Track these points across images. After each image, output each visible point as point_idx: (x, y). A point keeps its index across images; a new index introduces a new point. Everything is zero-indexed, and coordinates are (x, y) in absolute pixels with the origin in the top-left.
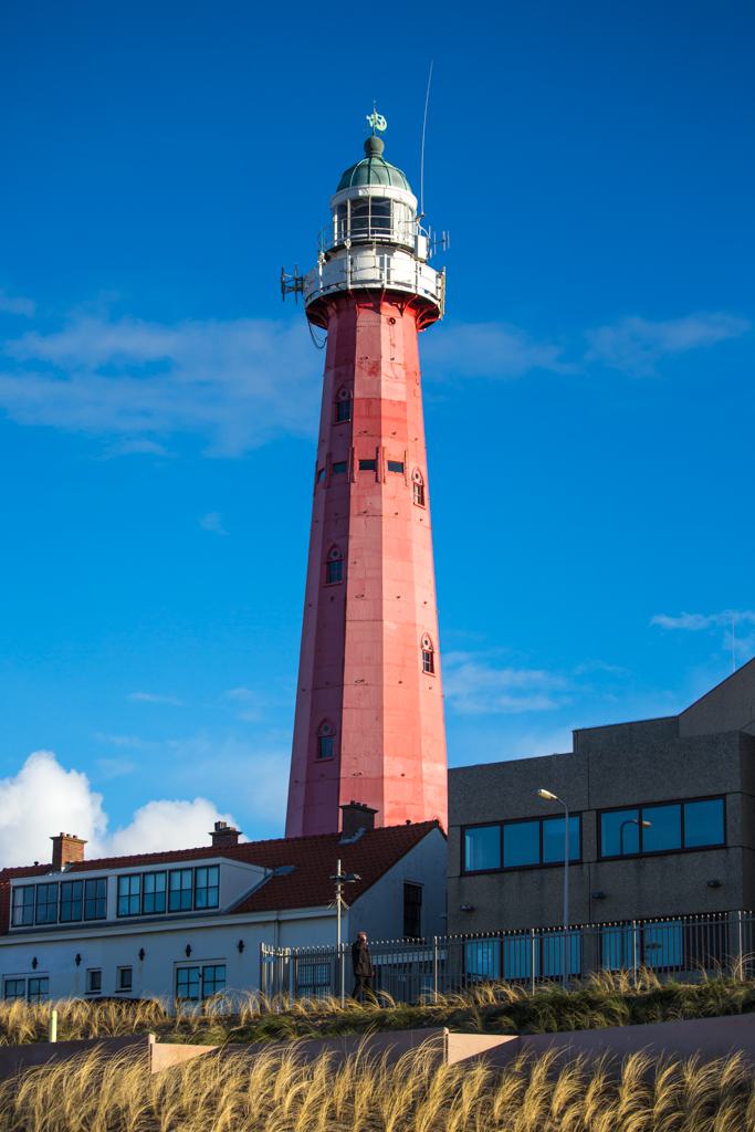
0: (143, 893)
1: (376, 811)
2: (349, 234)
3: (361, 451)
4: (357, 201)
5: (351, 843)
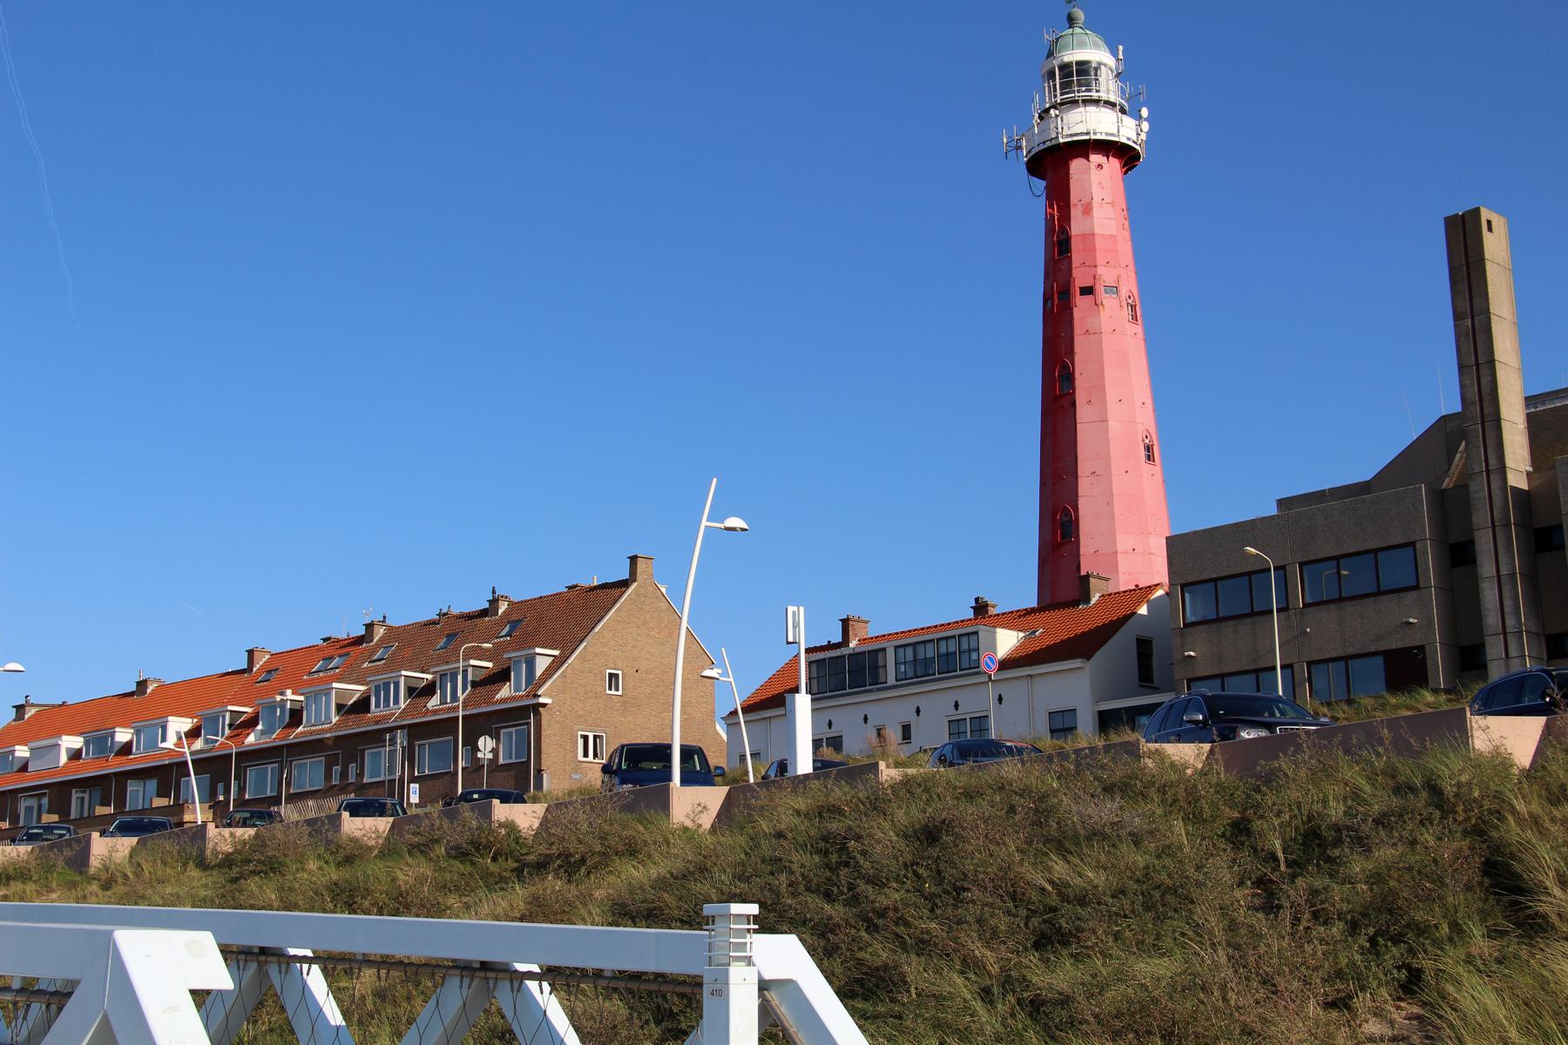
0: (915, 660)
2: (1058, 94)
3: (1080, 278)
4: (1065, 67)
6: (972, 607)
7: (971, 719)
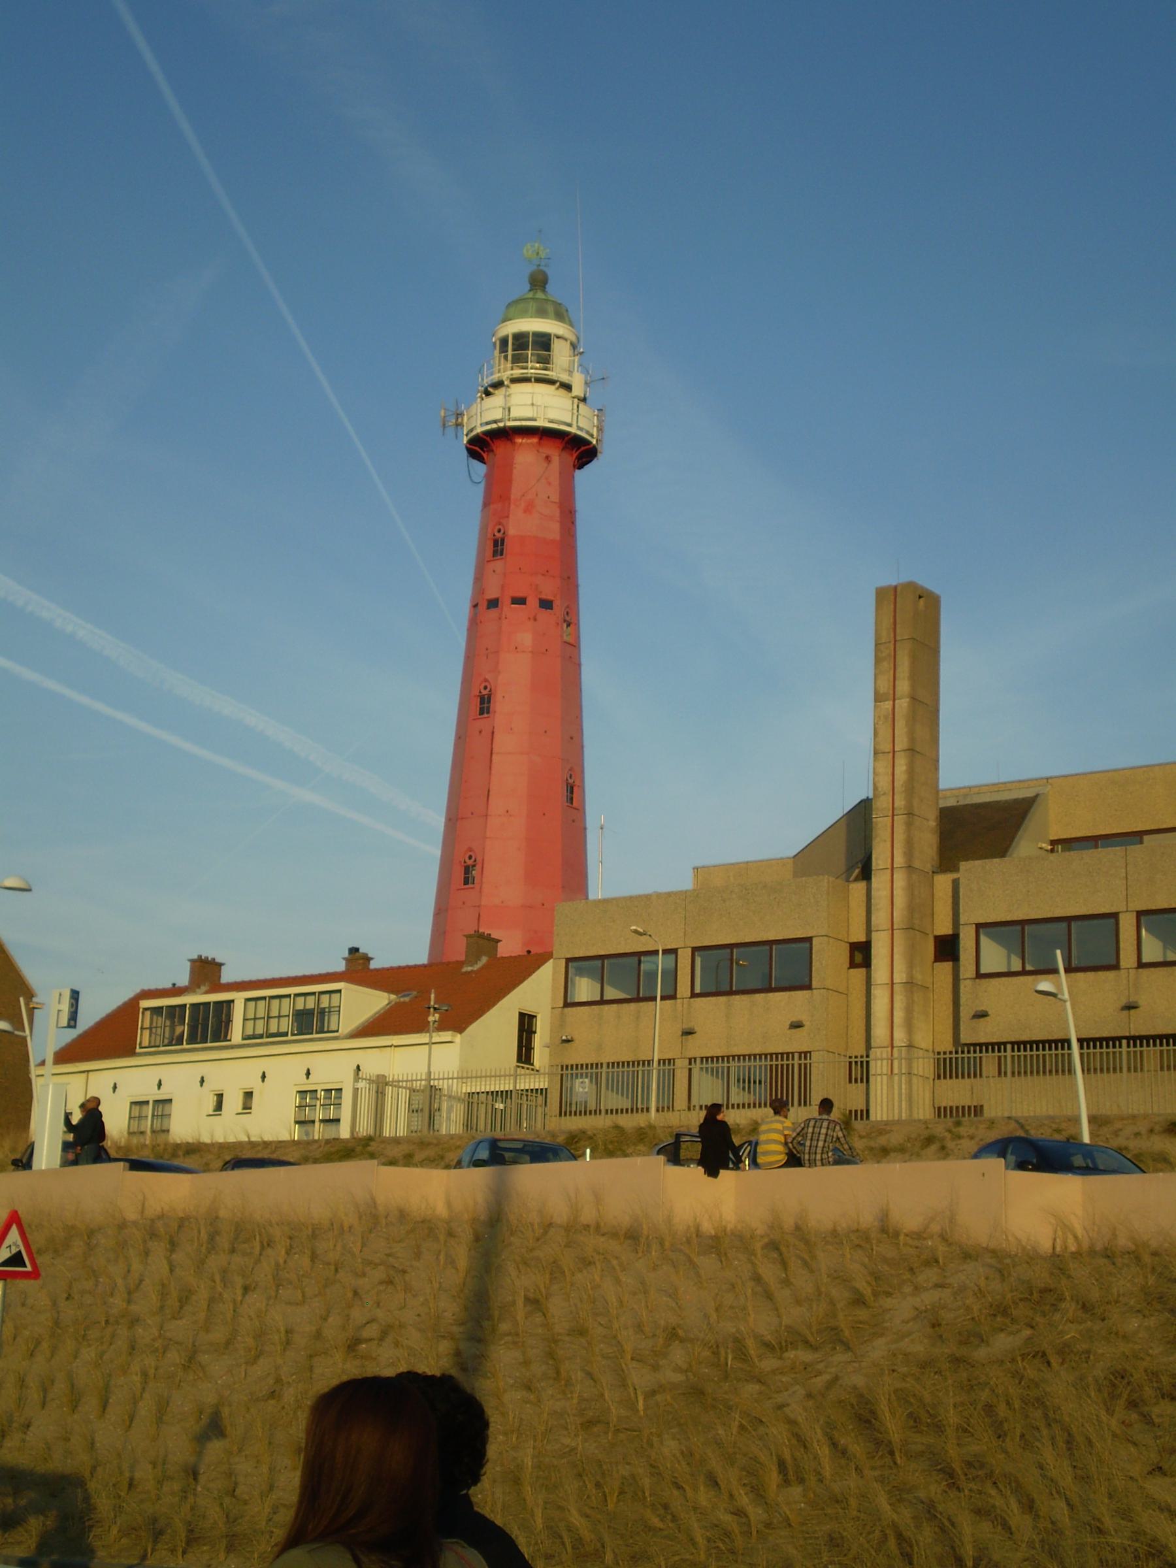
1: (500, 941)
5: (472, 971)
6: (344, 959)
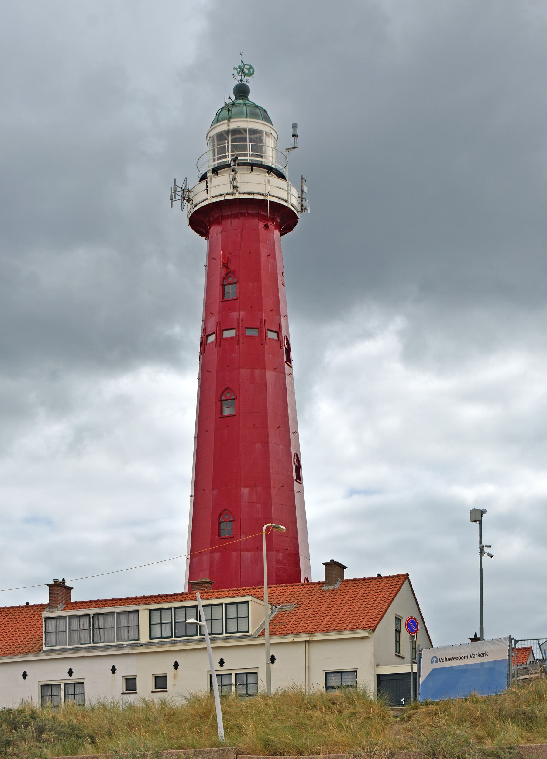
7: (236, 674)
